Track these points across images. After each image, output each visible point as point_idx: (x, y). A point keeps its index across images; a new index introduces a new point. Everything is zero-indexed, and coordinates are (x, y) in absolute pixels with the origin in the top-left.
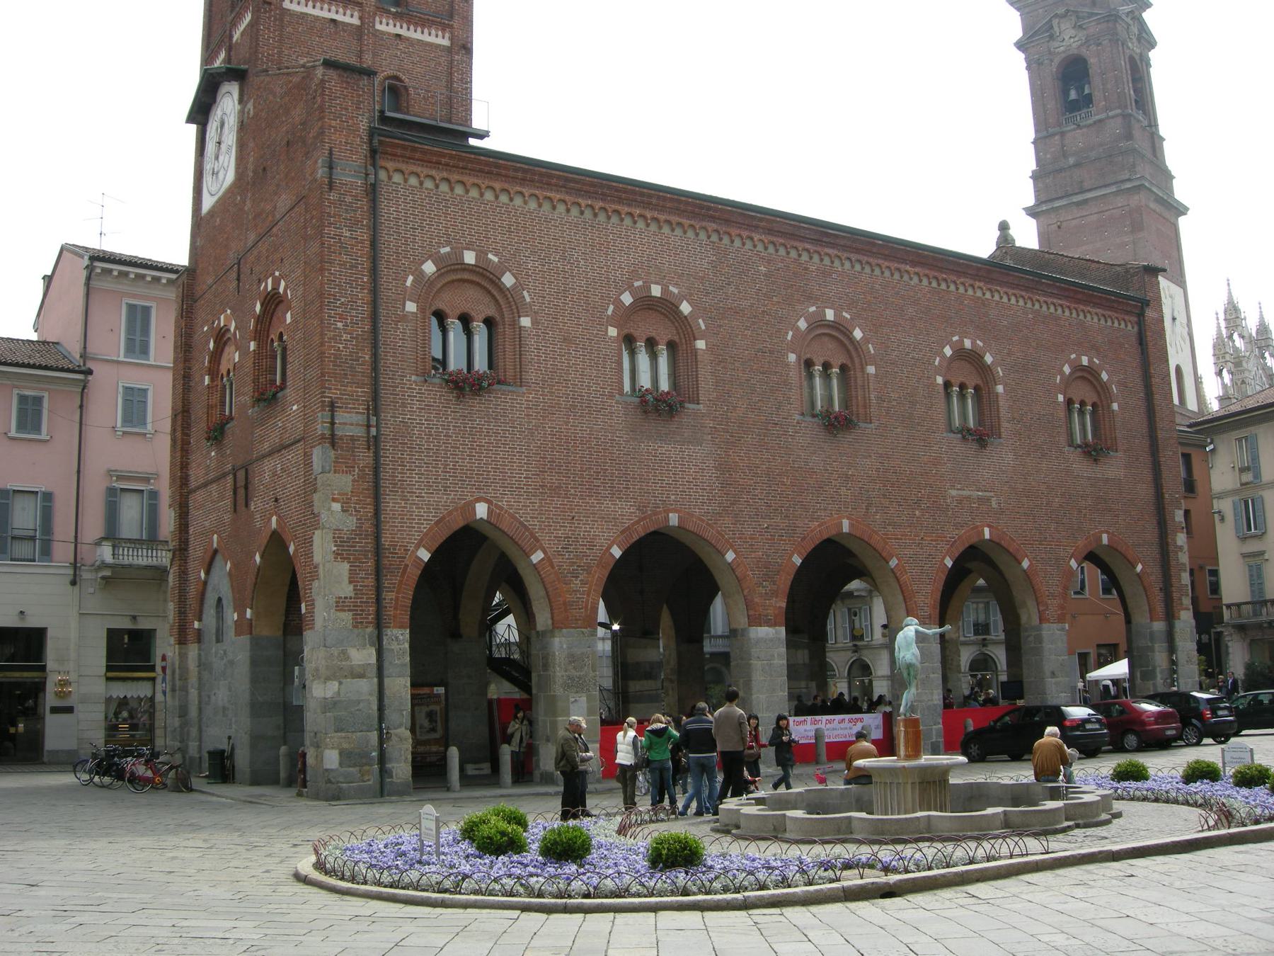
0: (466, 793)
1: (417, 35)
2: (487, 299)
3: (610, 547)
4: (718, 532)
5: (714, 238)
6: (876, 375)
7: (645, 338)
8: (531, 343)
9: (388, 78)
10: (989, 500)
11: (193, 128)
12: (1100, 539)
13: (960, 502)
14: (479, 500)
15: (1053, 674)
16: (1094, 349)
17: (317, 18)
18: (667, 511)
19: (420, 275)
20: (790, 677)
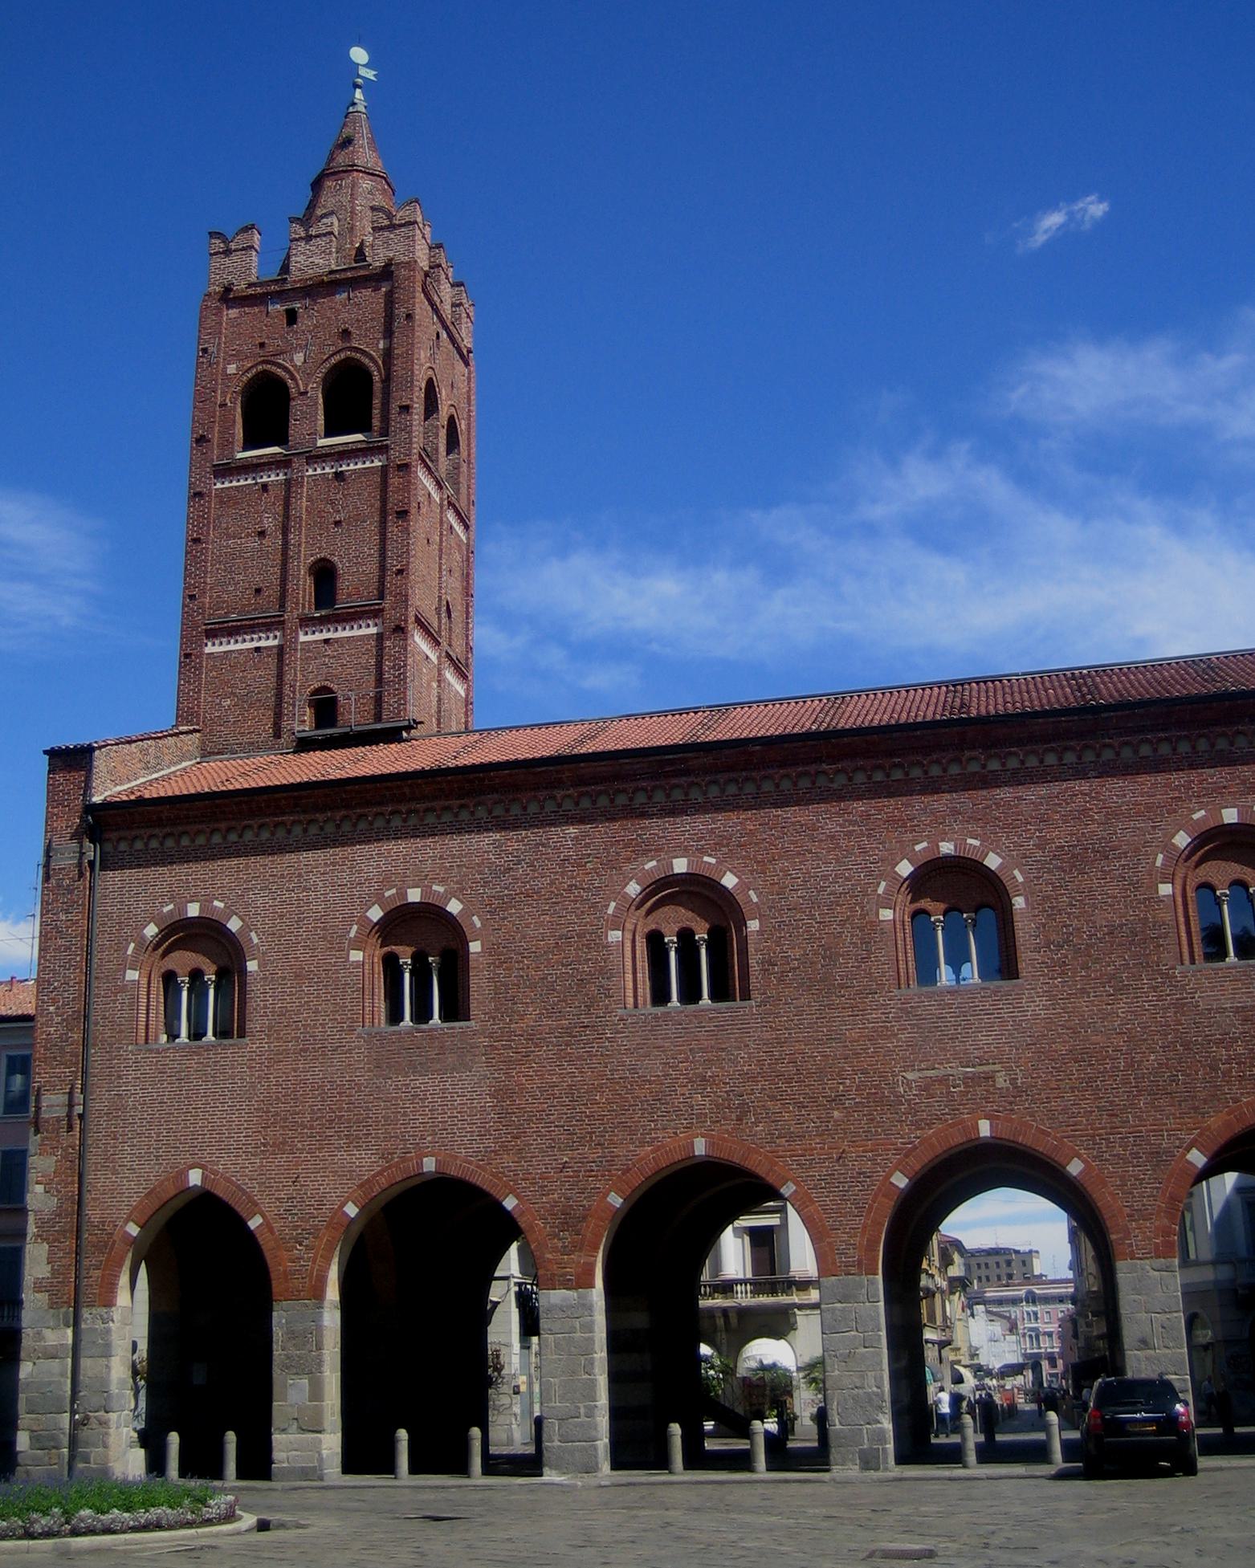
1: (347, 633)
3: (344, 1204)
6: (760, 932)
8: (255, 988)
9: (316, 692)
10: (990, 1077)
12: (183, 1175)
15: (1144, 1343)
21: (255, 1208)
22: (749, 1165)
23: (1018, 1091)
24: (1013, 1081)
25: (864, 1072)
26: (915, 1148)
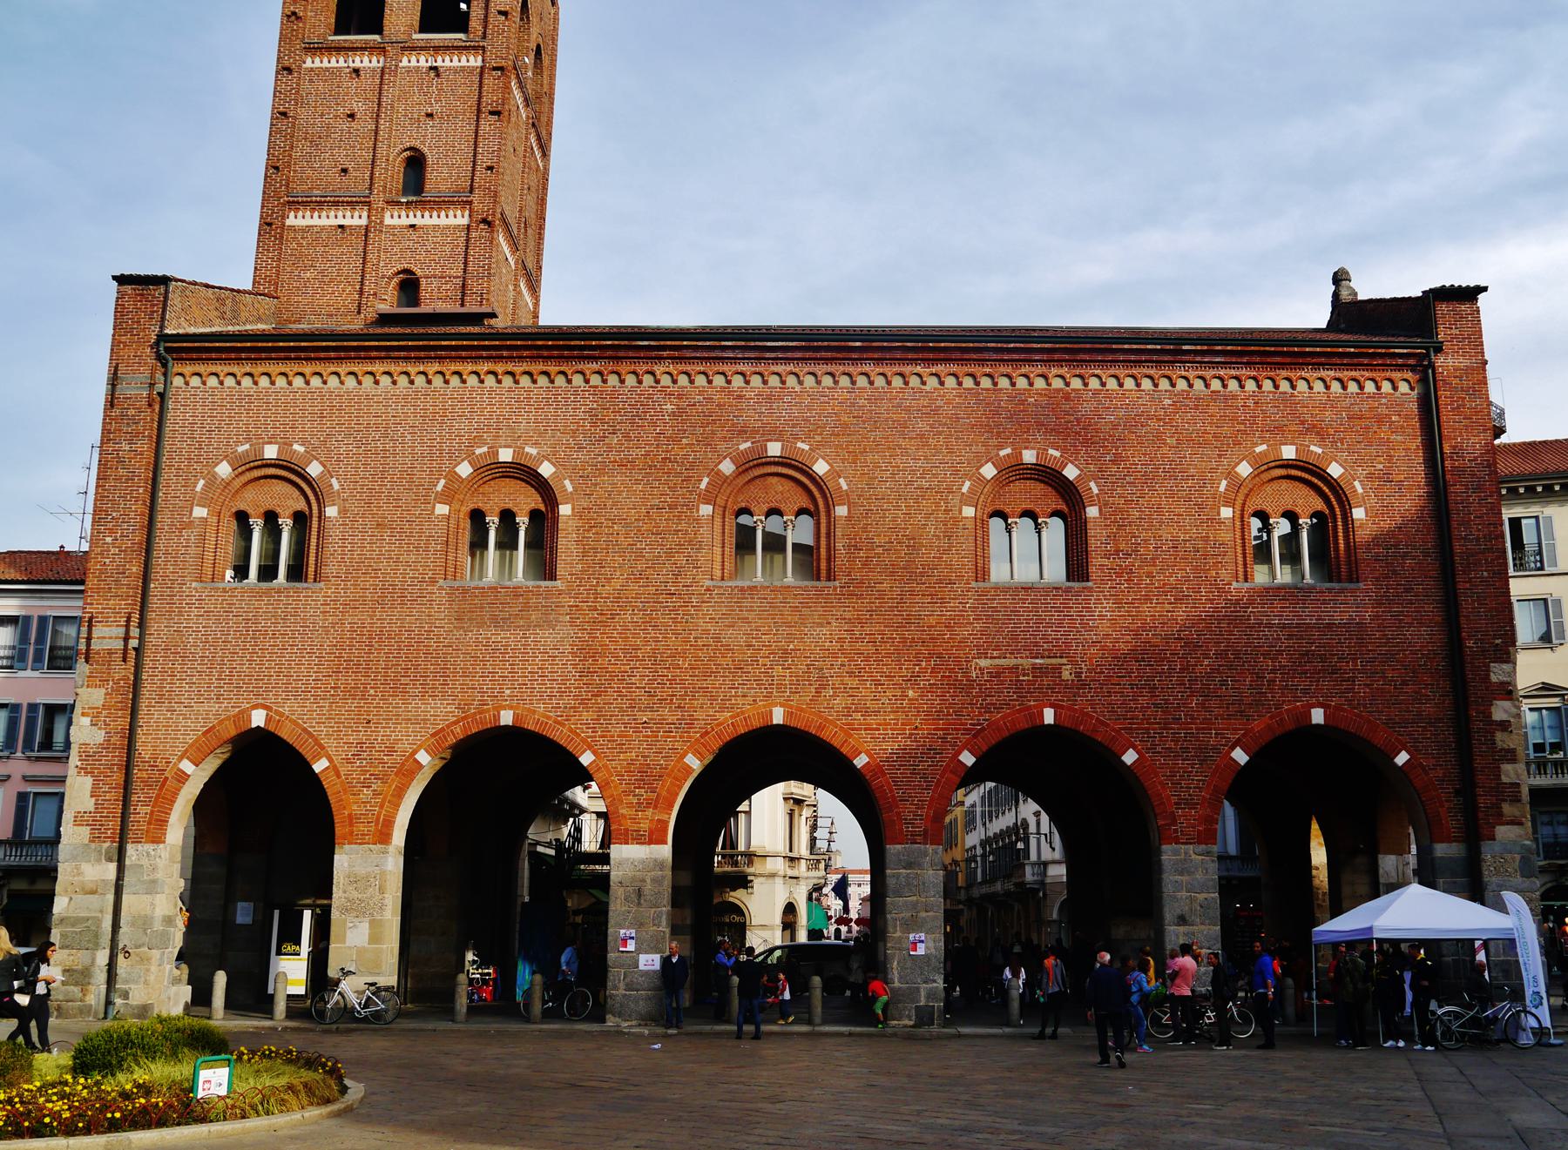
0: (476, 1026)
1: (435, 221)
2: (297, 493)
3: (415, 752)
4: (571, 730)
5: (595, 380)
6: (849, 518)
7: (497, 510)
8: (334, 534)
10: (1057, 669)
11: (1314, 314)
13: (998, 675)
14: (255, 707)
15: (1182, 920)
16: (1320, 433)
17: (323, 228)
18: (498, 709)
19: (212, 479)
20: (675, 903)
21: (321, 751)
22: (825, 735)
23: (1083, 685)
24: (1078, 674)
25: (940, 656)
26: (983, 729)
